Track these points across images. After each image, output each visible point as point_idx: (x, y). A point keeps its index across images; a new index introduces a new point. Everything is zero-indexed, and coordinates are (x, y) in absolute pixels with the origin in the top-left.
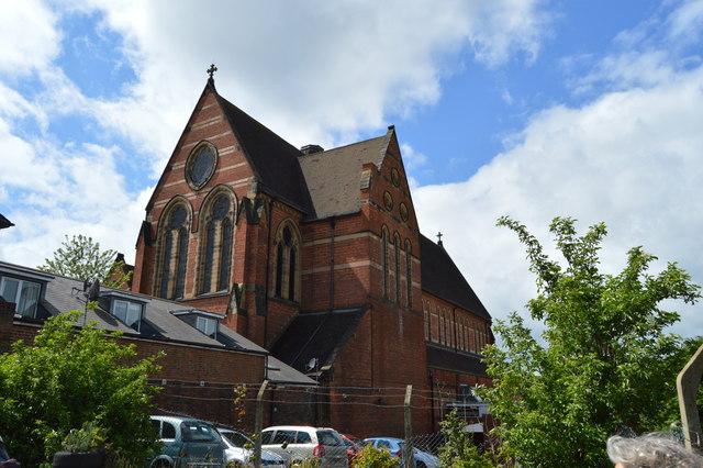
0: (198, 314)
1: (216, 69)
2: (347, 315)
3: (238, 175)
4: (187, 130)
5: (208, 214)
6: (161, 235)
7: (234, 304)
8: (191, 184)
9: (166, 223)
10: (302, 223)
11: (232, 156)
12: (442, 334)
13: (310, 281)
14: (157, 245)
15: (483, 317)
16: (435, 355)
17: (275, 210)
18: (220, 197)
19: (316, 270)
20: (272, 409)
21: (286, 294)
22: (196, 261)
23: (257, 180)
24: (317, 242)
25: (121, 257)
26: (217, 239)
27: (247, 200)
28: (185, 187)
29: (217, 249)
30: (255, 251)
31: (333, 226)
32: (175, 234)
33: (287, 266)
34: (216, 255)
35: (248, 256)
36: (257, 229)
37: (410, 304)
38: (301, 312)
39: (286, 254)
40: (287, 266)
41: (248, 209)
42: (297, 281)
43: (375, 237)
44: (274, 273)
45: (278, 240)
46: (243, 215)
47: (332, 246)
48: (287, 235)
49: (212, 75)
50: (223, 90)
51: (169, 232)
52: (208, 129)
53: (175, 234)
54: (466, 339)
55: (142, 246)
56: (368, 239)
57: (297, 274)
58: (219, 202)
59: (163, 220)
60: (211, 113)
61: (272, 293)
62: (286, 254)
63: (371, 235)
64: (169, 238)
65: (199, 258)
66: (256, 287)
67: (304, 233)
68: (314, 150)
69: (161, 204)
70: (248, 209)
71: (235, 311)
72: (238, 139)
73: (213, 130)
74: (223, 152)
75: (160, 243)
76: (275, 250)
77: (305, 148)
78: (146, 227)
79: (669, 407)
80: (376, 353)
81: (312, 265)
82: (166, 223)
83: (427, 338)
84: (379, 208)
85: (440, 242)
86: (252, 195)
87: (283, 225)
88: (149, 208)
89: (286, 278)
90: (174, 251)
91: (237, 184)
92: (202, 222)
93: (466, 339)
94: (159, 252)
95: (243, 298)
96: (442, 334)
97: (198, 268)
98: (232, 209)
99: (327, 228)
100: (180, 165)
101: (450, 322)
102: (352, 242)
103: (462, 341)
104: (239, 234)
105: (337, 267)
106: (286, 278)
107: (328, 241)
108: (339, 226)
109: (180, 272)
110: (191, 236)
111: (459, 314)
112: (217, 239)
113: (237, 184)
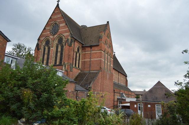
2: (94, 73)
3: (66, 32)
4: (50, 18)
8: (51, 34)
9: (44, 44)
10: (82, 47)
11: (64, 26)
12: (115, 79)
14: (41, 50)
17: (75, 43)
18: (48, 40)
19: (86, 60)
20: (77, 97)
21: (77, 66)
24: (86, 52)
26: (59, 49)
32: (47, 48)
34: (59, 54)
38: (81, 71)
39: (78, 55)
42: (80, 62)
43: (103, 52)
44: (75, 60)
45: (76, 51)
47: (90, 53)
49: (58, 3)
50: (60, 6)
51: (44, 47)
52: (57, 18)
53: (47, 48)
57: (80, 61)
59: (43, 43)
60: (58, 13)
61: (74, 66)
62: (78, 55)
63: (102, 51)
64: (45, 49)
67: (82, 49)
68: (84, 27)
73: (57, 19)
74: (61, 25)
76: (75, 54)
77: (82, 26)
78: (38, 45)
80: (102, 83)
84: (104, 44)
86: (70, 38)
87: (77, 47)
88: (39, 40)
89: (77, 62)
91: (65, 34)
95: (67, 67)
96: (115, 79)
97: (53, 58)
98: (63, 41)
99: (89, 49)
101: (117, 76)
102: (96, 53)
105: (92, 60)
106: (77, 62)
107: (90, 52)
108: (93, 48)
109: (48, 59)
110: (51, 48)
111: (119, 74)
112: (59, 49)
113: (65, 34)
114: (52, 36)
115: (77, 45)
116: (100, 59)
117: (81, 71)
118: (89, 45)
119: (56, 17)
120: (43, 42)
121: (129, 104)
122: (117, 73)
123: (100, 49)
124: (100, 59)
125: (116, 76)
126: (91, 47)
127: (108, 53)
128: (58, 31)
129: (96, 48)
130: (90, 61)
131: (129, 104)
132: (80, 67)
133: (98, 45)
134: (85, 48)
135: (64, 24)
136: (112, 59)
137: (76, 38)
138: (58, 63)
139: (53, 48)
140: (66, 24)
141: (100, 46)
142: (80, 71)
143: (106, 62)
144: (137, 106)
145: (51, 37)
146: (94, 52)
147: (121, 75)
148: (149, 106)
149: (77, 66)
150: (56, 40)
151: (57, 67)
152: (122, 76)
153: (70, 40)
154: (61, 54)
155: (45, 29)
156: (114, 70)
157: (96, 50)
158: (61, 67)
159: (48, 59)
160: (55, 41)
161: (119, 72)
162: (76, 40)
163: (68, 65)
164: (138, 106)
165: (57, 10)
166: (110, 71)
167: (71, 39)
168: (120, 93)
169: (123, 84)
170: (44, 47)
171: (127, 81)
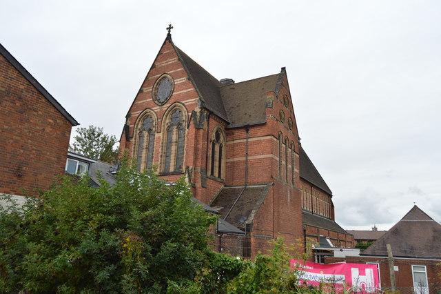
1: (172, 28)
3: (188, 96)
4: (153, 66)
5: (167, 121)
7: (187, 180)
9: (139, 126)
10: (227, 129)
13: (231, 167)
14: (133, 140)
15: (329, 195)
18: (148, 116)
19: (236, 159)
21: (216, 174)
22: (160, 150)
24: (236, 142)
26: (174, 137)
28: (153, 104)
29: (174, 144)
31: (247, 131)
32: (146, 134)
33: (217, 156)
34: (174, 148)
35: (196, 149)
36: (201, 131)
39: (217, 148)
40: (217, 156)
41: (195, 119)
42: (223, 165)
43: (275, 139)
44: (210, 161)
49: (169, 31)
51: (141, 132)
53: (146, 134)
56: (272, 141)
58: (174, 110)
59: (138, 124)
60: (170, 56)
61: (209, 173)
62: (217, 148)
65: (162, 149)
66: (201, 169)
68: (229, 82)
69: (136, 114)
74: (178, 81)
75: (135, 139)
76: (211, 146)
77: (222, 81)
78: (126, 128)
81: (233, 156)
82: (139, 126)
86: (198, 110)
87: (215, 130)
88: (128, 116)
89: (217, 164)
90: (173, 157)
91: (188, 102)
92: (164, 126)
94: (135, 144)
97: (161, 156)
99: (243, 133)
100: (148, 89)
102: (259, 142)
103: (305, 202)
104: (190, 132)
105: (249, 158)
106: (217, 164)
107: (245, 140)
108: (251, 131)
110: (157, 135)
112: (174, 137)
113: (188, 102)
114: (158, 107)
115: (214, 125)
116: (271, 156)
117: (225, 186)
118: (241, 124)
119: (165, 63)
120: (139, 121)
121: (353, 269)
123: (268, 133)
124: (271, 156)
126: (247, 128)
128: (170, 96)
129: (259, 131)
130: (246, 162)
131: (353, 269)
132: (222, 176)
133: (264, 124)
134: (234, 131)
135: (183, 80)
137: (211, 109)
138: (172, 169)
139: (161, 135)
140: (189, 79)
141: (269, 124)
142: (222, 186)
145: (157, 109)
146: (256, 139)
147: (318, 192)
149: (216, 174)
150: (167, 116)
151: (172, 177)
152: (321, 195)
153: (198, 114)
154: (180, 148)
155: (141, 91)
156: (301, 185)
157: (259, 134)
160: (166, 119)
161: (312, 185)
162: (211, 113)
163: (195, 173)
165: (168, 49)
167: (201, 112)
169: (323, 214)
170: (141, 132)
171: (333, 206)
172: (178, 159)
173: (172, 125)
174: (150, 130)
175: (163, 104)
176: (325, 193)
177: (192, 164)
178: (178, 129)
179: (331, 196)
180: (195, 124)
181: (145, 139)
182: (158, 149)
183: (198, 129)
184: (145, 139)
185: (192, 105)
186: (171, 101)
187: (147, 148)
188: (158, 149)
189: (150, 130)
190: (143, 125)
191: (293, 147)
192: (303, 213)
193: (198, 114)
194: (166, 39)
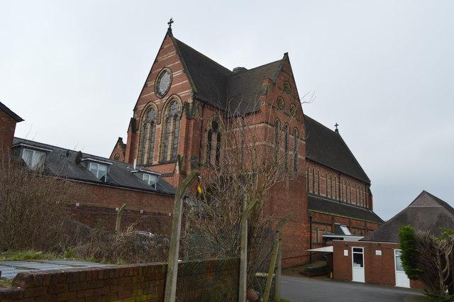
0: (144, 172)
3: (183, 88)
4: (156, 61)
5: (166, 113)
6: (141, 127)
7: (177, 167)
9: (144, 119)
11: (180, 76)
12: (329, 190)
14: (139, 132)
15: (365, 182)
16: (313, 203)
23: (193, 91)
25: (120, 139)
26: (171, 128)
27: (187, 104)
28: (155, 97)
29: (171, 134)
30: (191, 135)
32: (149, 126)
34: (170, 138)
35: (187, 139)
37: (296, 170)
39: (214, 136)
41: (188, 110)
45: (208, 128)
46: (184, 113)
48: (215, 125)
49: (170, 26)
50: (176, 35)
51: (145, 124)
53: (149, 126)
54: (349, 193)
55: (131, 133)
60: (169, 50)
62: (214, 136)
68: (241, 71)
69: (141, 107)
70: (188, 110)
71: (178, 172)
72: (184, 66)
74: (176, 74)
76: (206, 135)
78: (133, 122)
79: (105, 201)
82: (144, 119)
83: (311, 192)
85: (337, 130)
86: (190, 101)
89: (214, 152)
91: (183, 94)
93: (349, 193)
95: (183, 164)
96: (329, 190)
100: (152, 83)
101: (335, 183)
103: (345, 195)
109: (151, 149)
110: (158, 126)
113: (183, 94)
114: (159, 100)
119: (165, 57)
122: (336, 176)
125: (326, 185)
127: (279, 124)
136: (305, 143)
137: (205, 99)
138: (169, 159)
139: (160, 126)
140: (184, 72)
143: (282, 149)
144: (350, 253)
145: (158, 101)
147: (349, 181)
148: (379, 253)
153: (191, 105)
155: (145, 85)
156: (311, 167)
158: (173, 165)
159: (151, 149)
161: (340, 173)
164: (353, 252)
165: (169, 43)
166: (296, 170)
167: (193, 103)
168: (331, 225)
169: (356, 202)
171: (370, 195)
172: (174, 149)
173: (171, 116)
174: (153, 122)
175: (164, 96)
176: (360, 181)
177: (183, 153)
178: (175, 119)
179: (369, 185)
180: (187, 114)
181: (149, 130)
182: (158, 139)
183: (189, 119)
184: (149, 130)
185: (185, 96)
186: (169, 93)
187: (149, 139)
188: (158, 139)
189: (153, 122)
190: (147, 117)
191: (297, 133)
192: (308, 197)
193: (191, 105)
194: (167, 34)
